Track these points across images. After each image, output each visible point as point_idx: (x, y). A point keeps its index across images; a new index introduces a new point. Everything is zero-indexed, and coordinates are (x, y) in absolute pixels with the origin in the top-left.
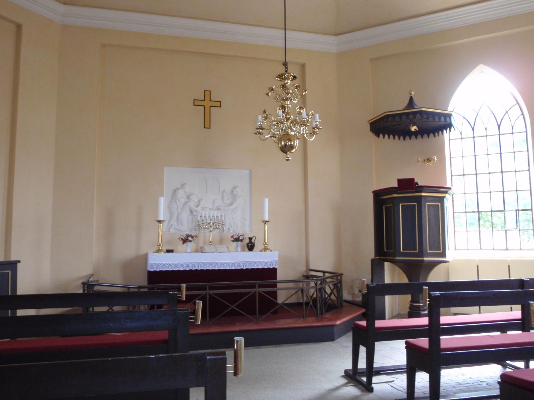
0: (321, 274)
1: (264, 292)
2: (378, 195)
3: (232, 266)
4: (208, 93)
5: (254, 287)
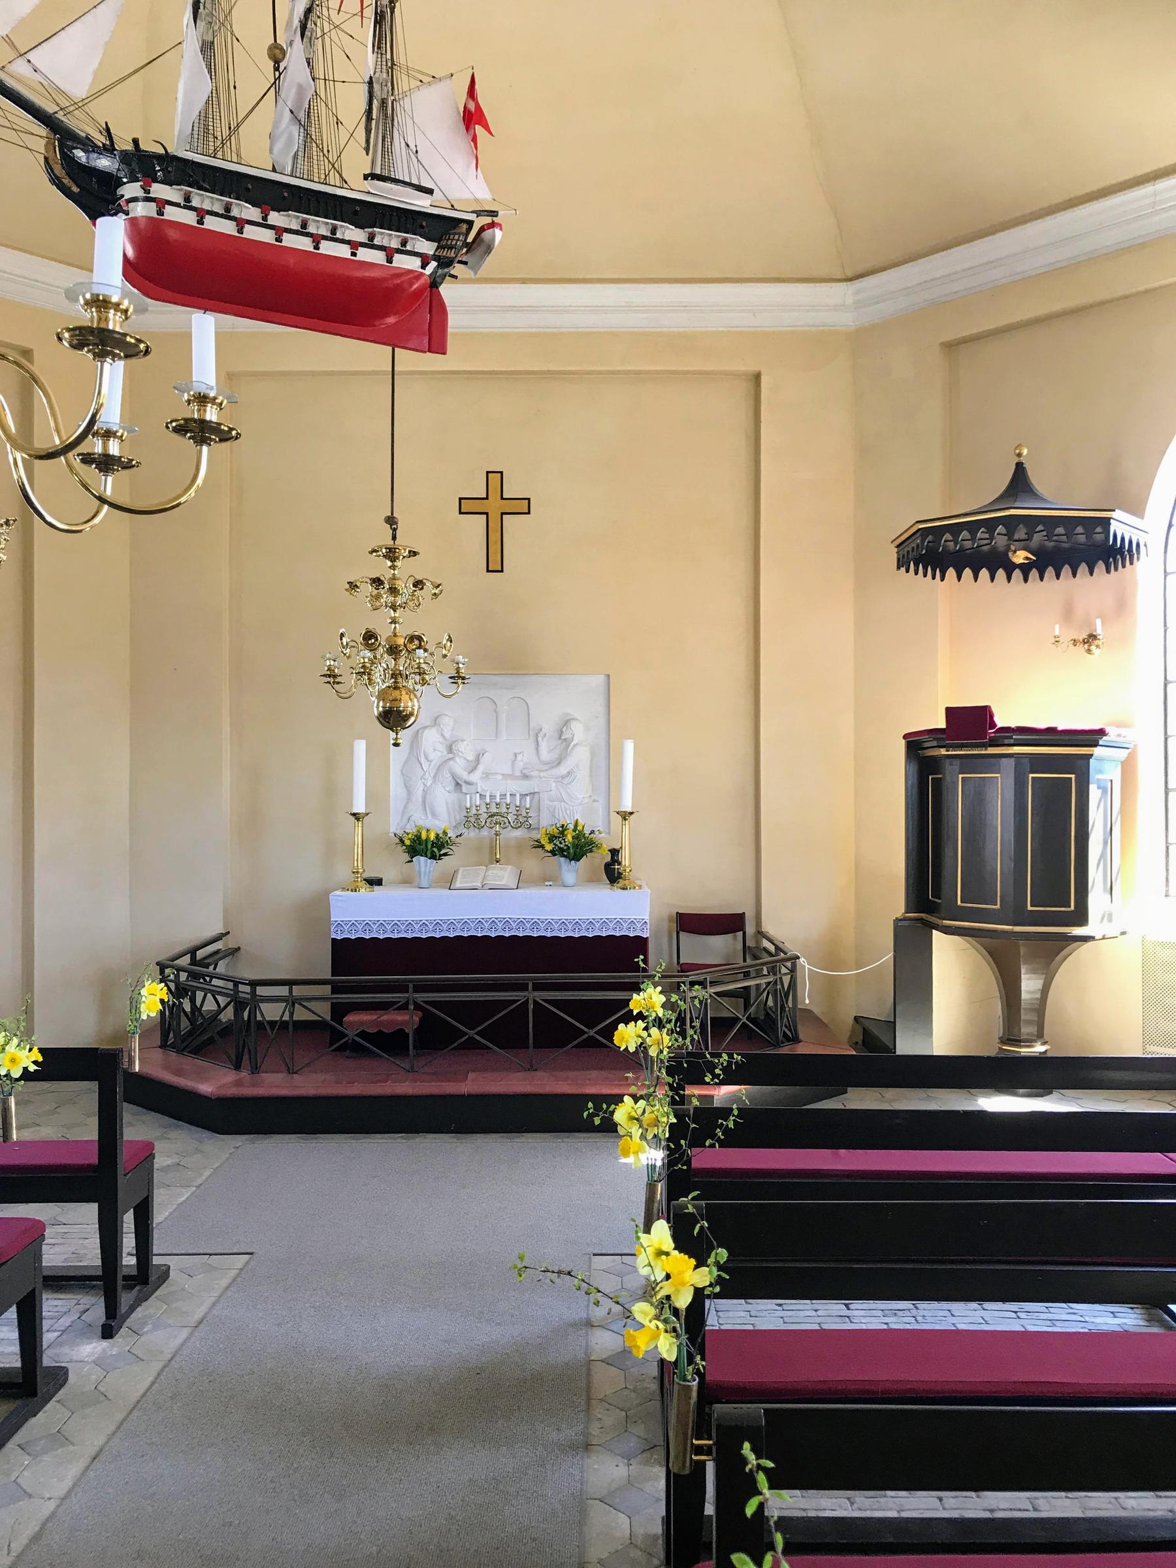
1: (545, 1001)
2: (915, 744)
4: (495, 477)
5: (523, 987)
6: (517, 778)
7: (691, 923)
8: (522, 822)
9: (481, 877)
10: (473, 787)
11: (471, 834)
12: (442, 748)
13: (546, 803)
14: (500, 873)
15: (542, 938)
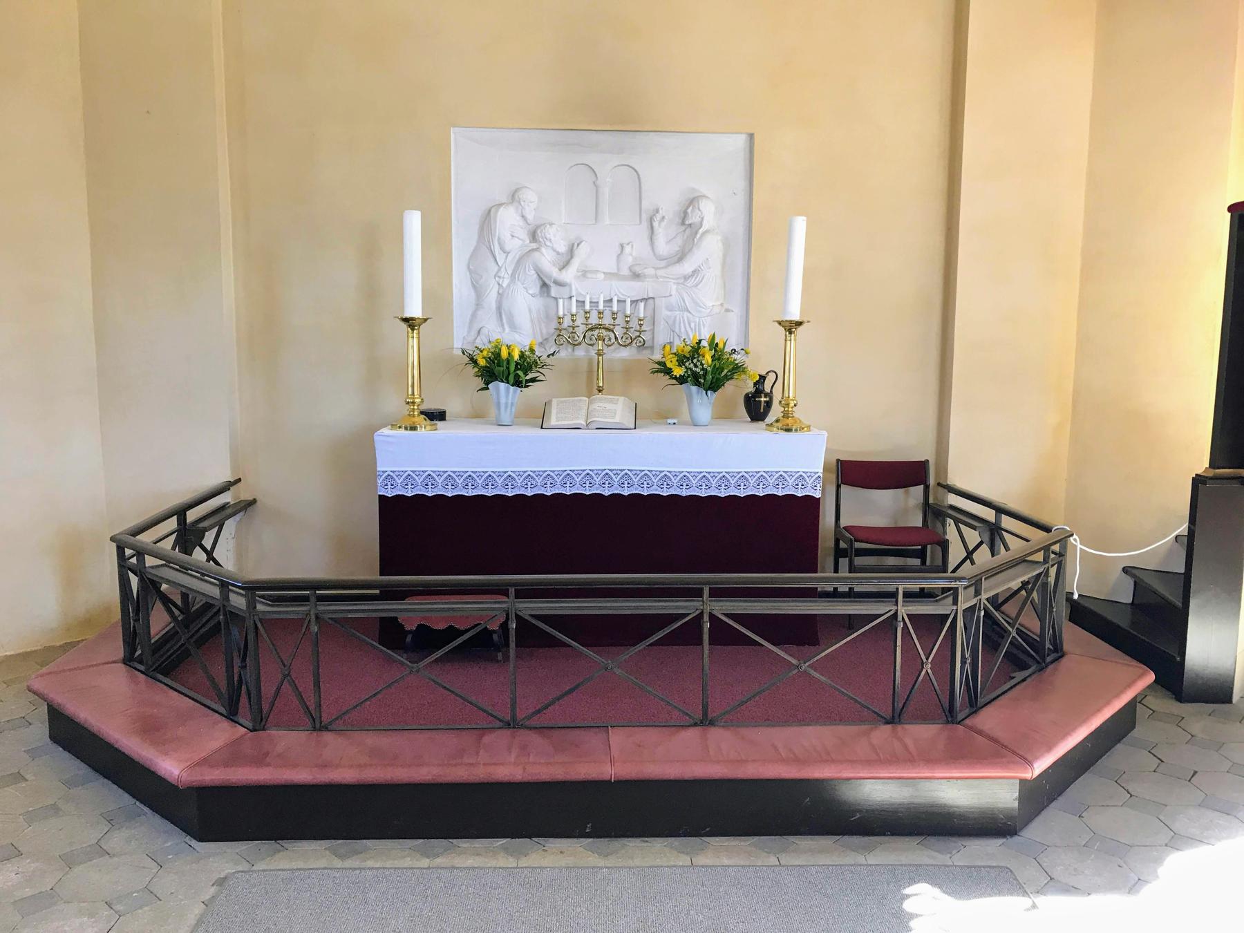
0: (989, 515)
3: (525, 486)
6: (624, 278)
7: (853, 473)
8: (634, 339)
9: (584, 412)
10: (567, 289)
11: (564, 353)
12: (523, 235)
13: (663, 313)
14: (609, 406)
15: (674, 498)
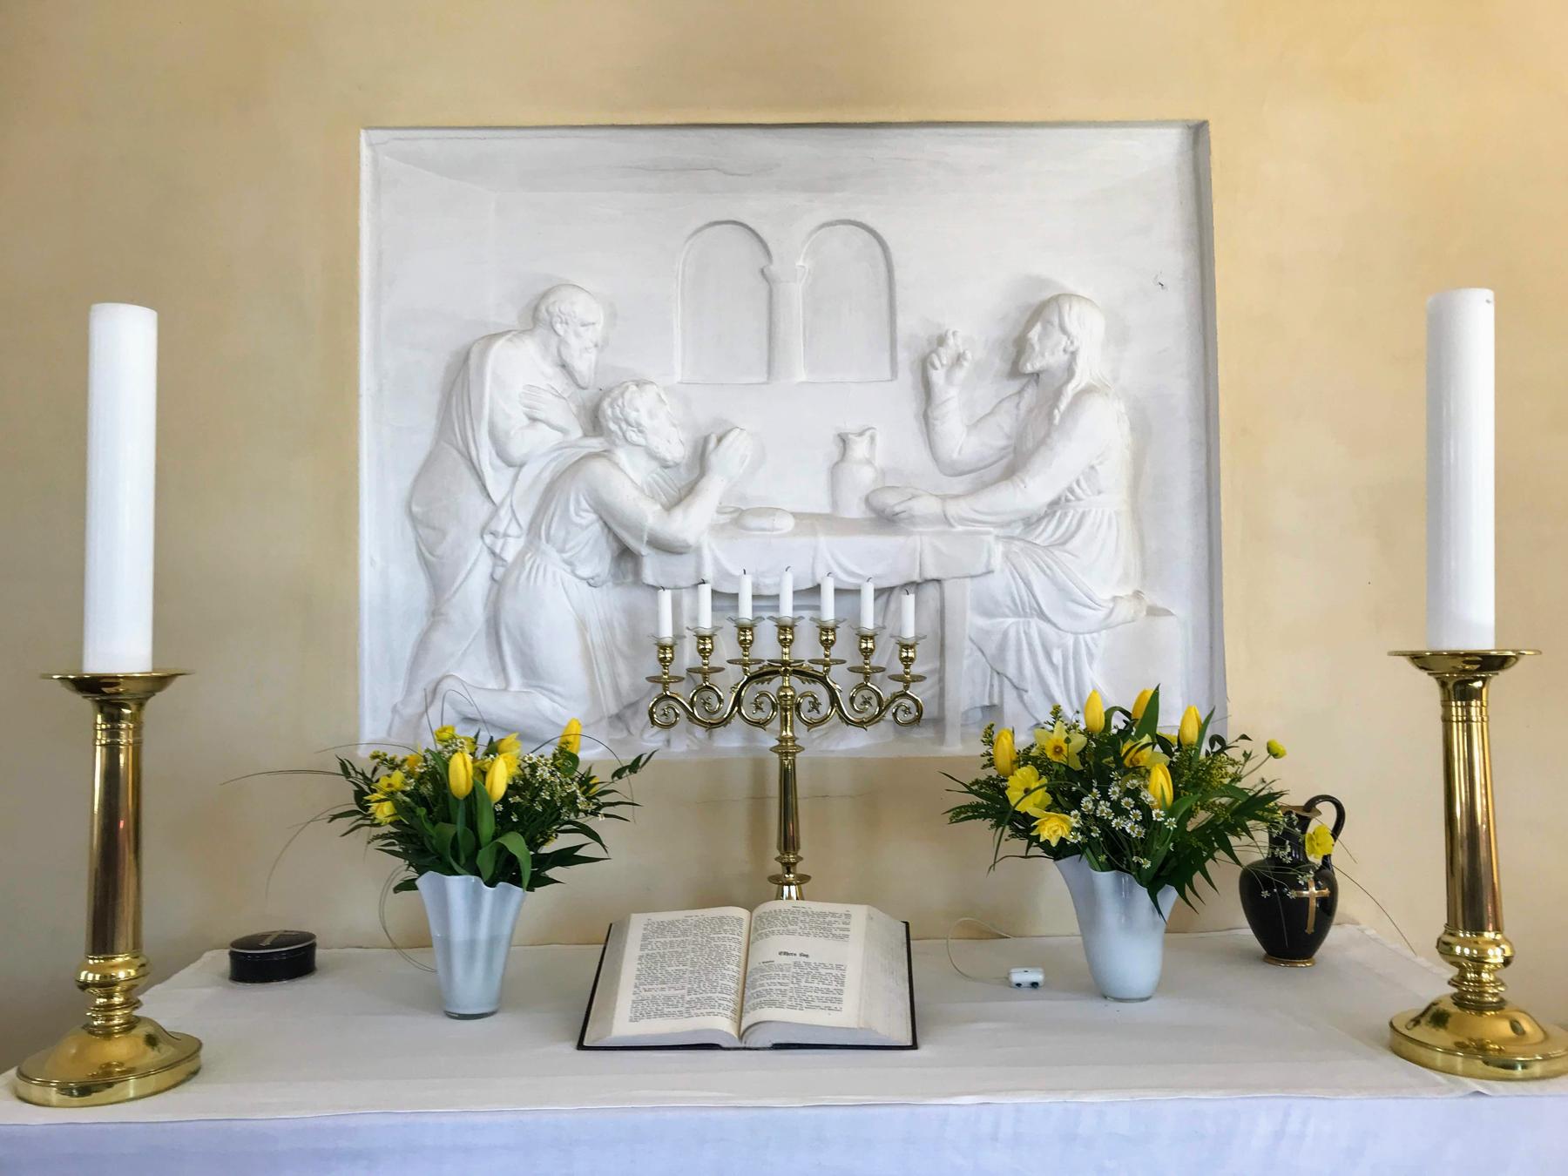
8: (894, 695)
12: (562, 414)
13: (968, 623)
14: (818, 949)
